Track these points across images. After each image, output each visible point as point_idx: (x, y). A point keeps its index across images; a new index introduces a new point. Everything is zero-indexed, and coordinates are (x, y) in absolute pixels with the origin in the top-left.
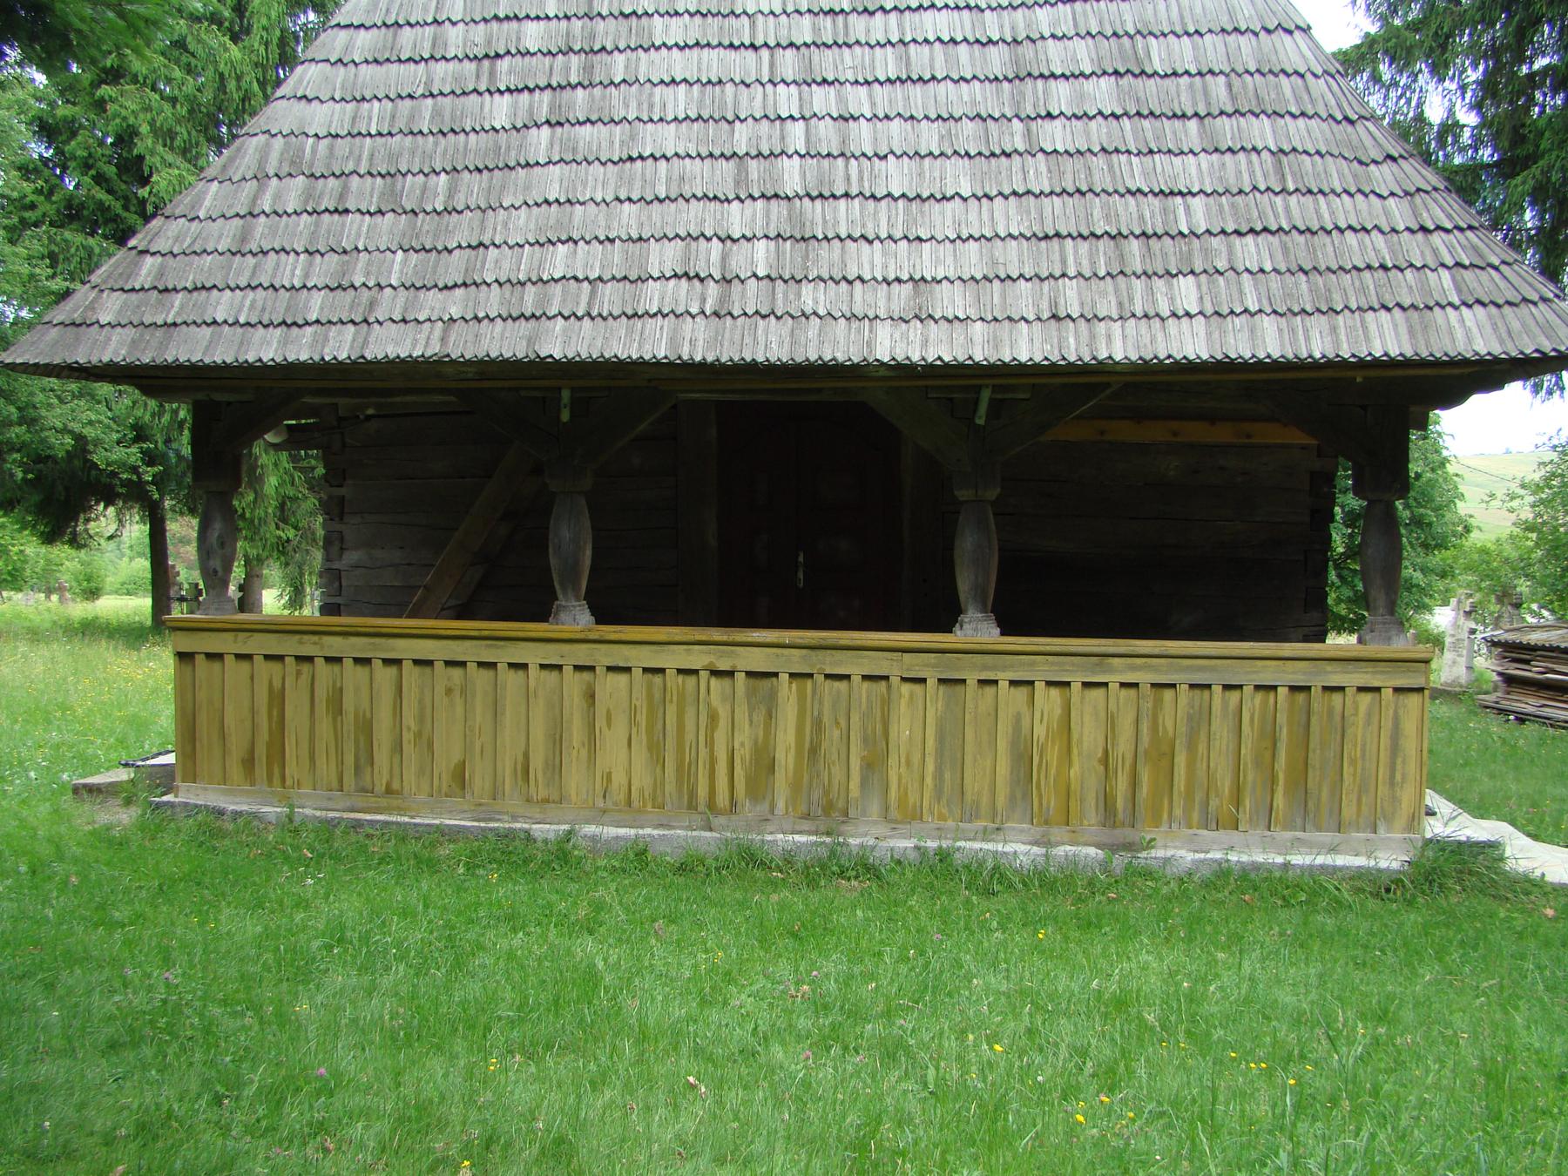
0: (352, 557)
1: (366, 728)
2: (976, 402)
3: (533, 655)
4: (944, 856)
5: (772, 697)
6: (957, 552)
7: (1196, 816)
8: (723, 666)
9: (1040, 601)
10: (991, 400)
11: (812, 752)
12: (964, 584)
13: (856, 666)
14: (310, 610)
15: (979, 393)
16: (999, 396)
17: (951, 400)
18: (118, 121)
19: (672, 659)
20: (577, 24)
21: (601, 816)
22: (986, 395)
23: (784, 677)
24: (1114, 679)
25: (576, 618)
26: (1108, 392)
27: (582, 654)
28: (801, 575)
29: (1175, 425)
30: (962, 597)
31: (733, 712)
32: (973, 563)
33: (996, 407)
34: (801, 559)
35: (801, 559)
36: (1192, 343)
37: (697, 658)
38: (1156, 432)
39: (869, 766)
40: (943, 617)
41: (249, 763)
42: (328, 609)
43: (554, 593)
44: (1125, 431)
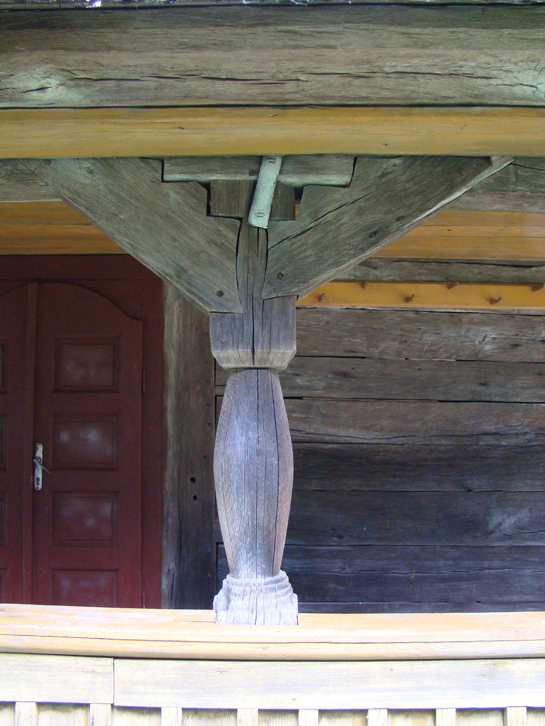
2: (253, 188)
6: (218, 463)
7: (302, 333)
10: (278, 185)
12: (233, 522)
15: (256, 172)
16: (295, 180)
17: (207, 186)
22: (269, 175)
26: (485, 175)
28: (39, 474)
29: (493, 290)
30: (230, 546)
31: (329, 357)
33: (289, 199)
34: (40, 453)
35: (40, 453)
38: (468, 299)
40: (200, 583)
44: (433, 298)
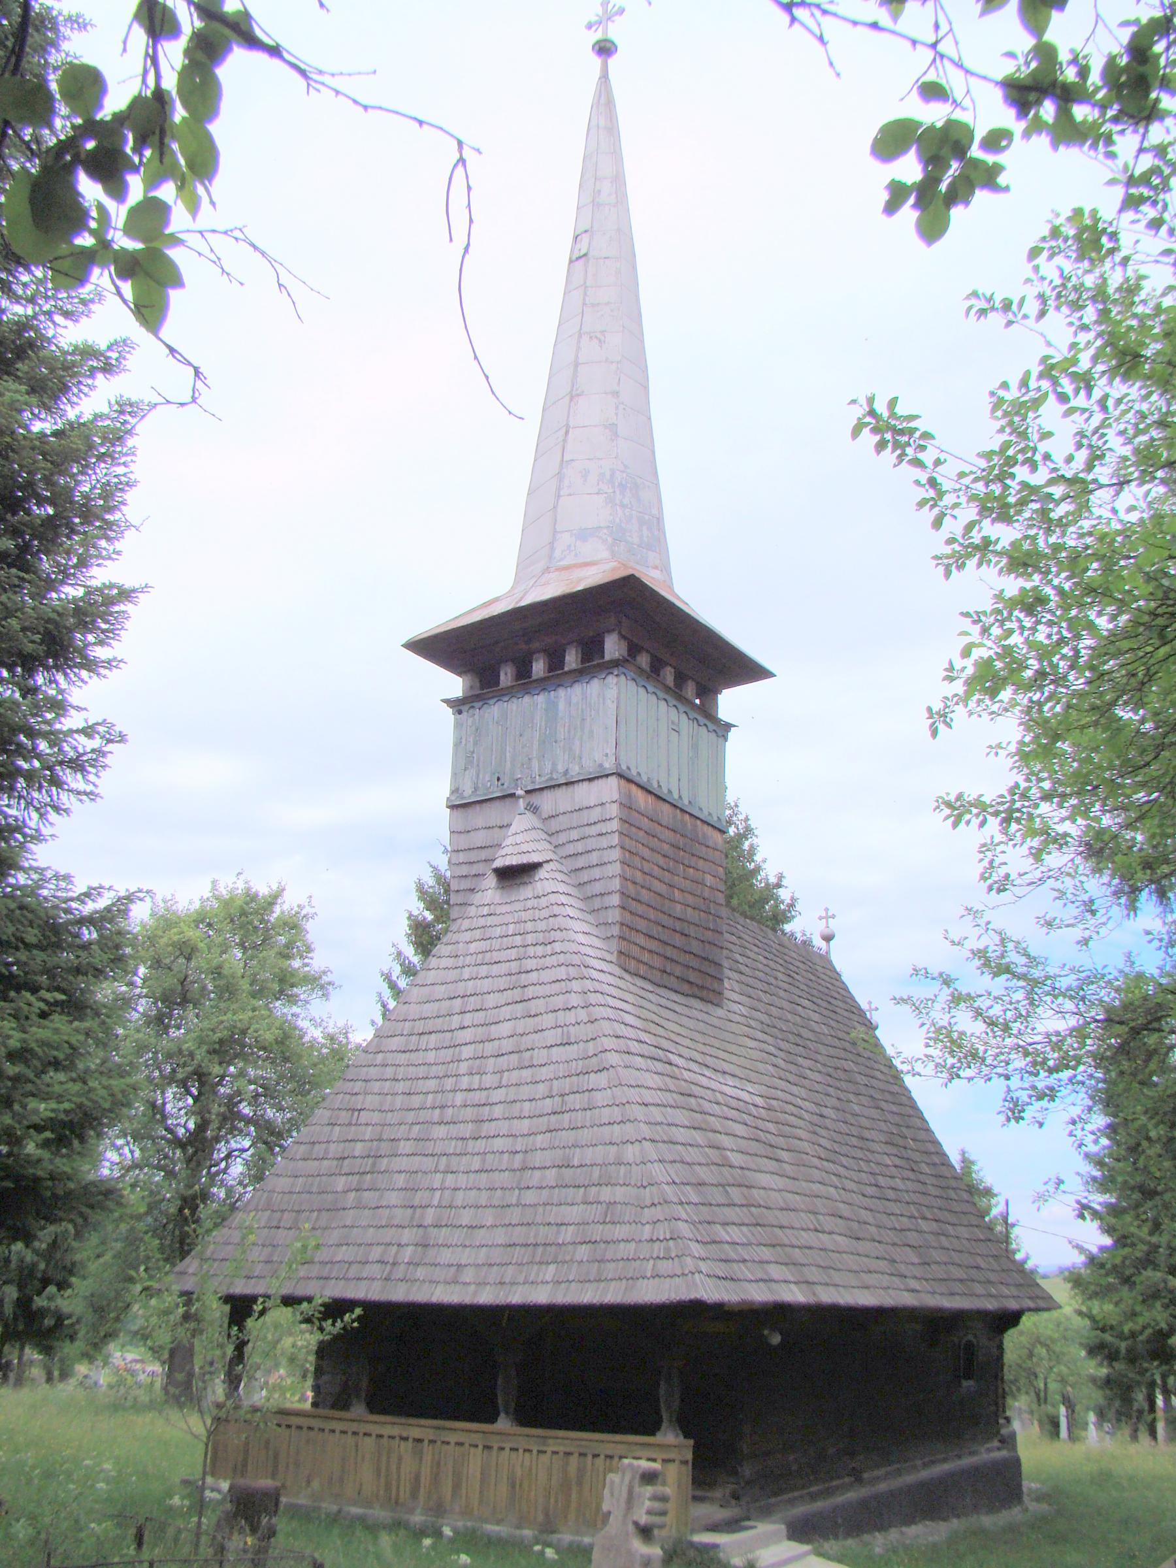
0: (325, 1378)
1: (276, 1456)
3: (338, 1426)
4: (474, 1531)
5: (421, 1452)
8: (405, 1434)
9: (536, 1412)
11: (436, 1479)
13: (453, 1438)
14: (307, 1406)
18: (66, 1295)
19: (387, 1430)
20: (375, 1143)
21: (355, 1504)
23: (426, 1442)
24: (549, 1449)
25: (504, 1423)
27: (354, 1427)
32: (505, 1390)
36: (541, 1296)
37: (395, 1431)
39: (457, 1486)
41: (235, 1468)
42: (315, 1404)
43: (658, 1412)
